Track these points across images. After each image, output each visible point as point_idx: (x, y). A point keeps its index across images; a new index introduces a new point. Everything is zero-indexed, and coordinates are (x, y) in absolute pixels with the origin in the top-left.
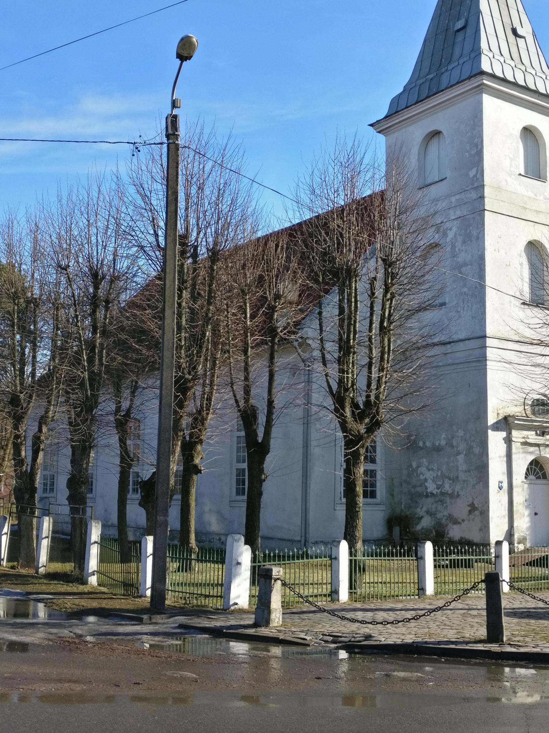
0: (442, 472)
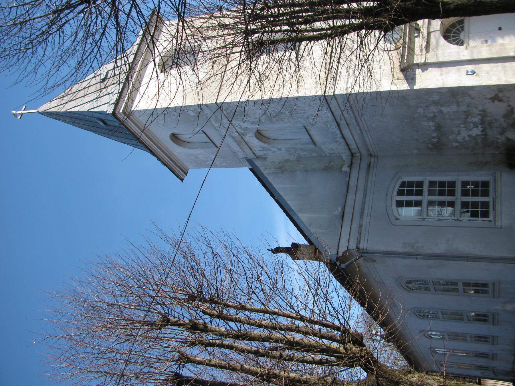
0: (460, 124)
